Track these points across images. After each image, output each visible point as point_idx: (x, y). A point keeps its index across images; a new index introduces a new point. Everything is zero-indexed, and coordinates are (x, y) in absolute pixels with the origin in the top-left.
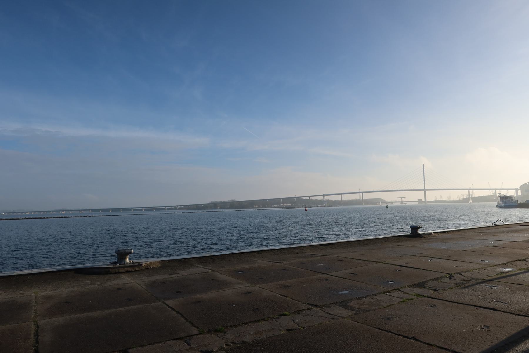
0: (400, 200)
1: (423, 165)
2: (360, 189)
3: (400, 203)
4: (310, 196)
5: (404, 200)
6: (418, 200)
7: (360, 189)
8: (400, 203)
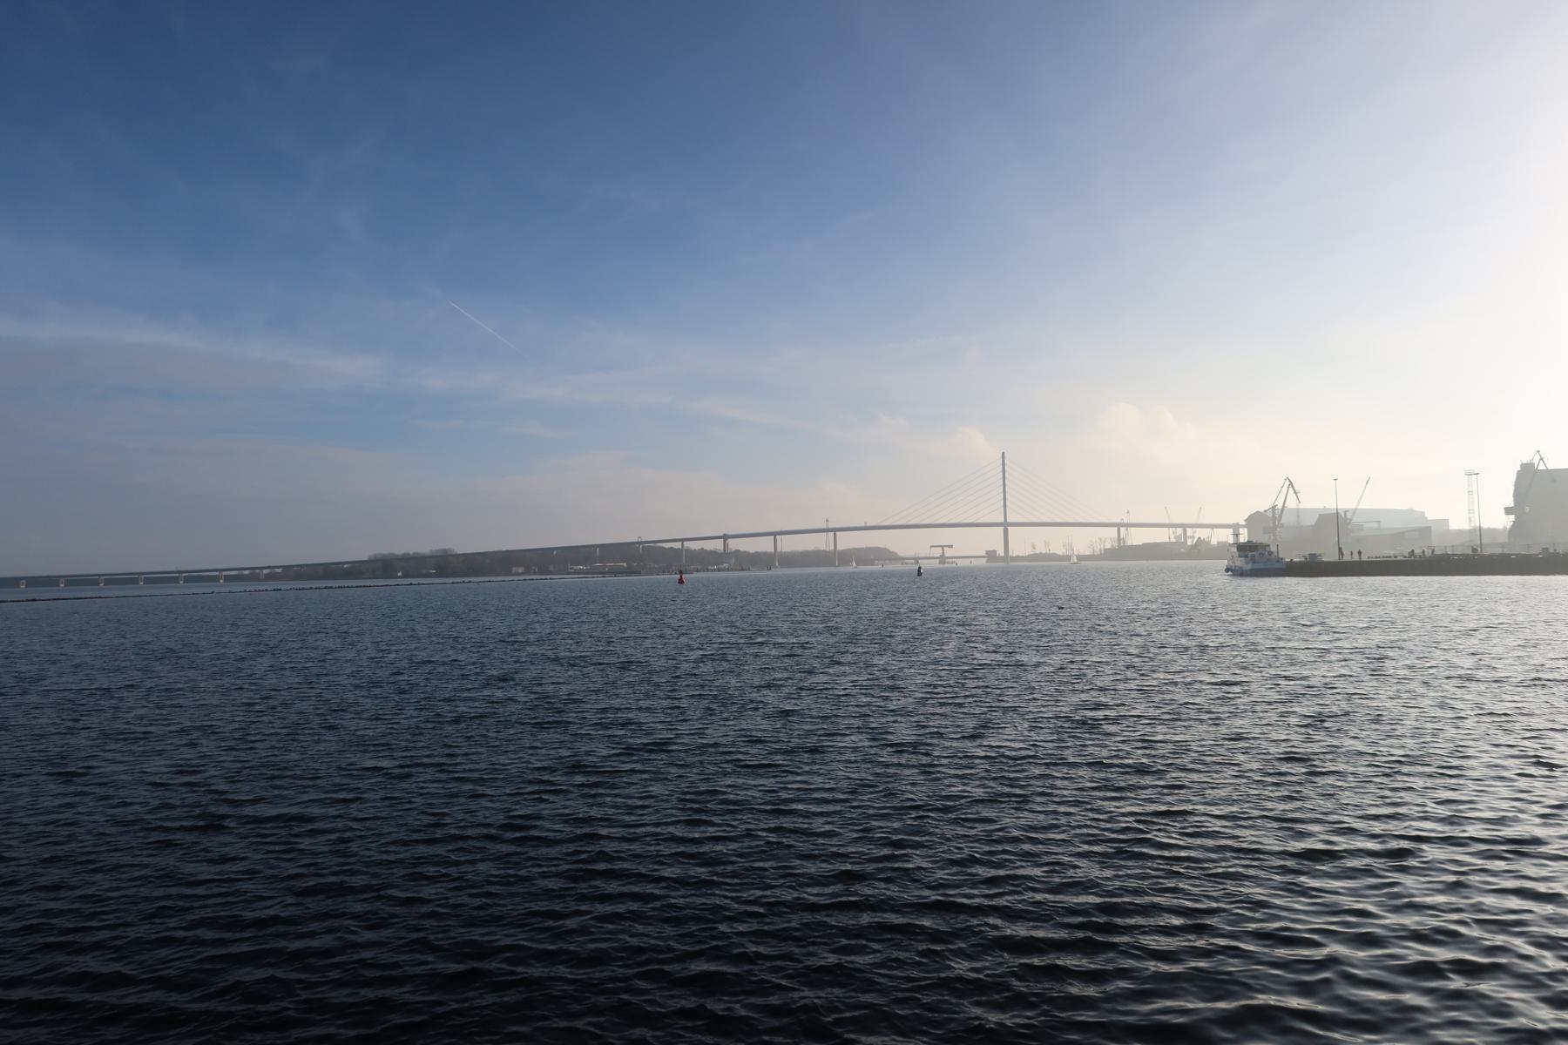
0: (937, 552)
1: (1003, 454)
2: (827, 521)
3: (938, 561)
4: (683, 540)
5: (948, 552)
6: (987, 552)
7: (827, 521)
8: (938, 561)
